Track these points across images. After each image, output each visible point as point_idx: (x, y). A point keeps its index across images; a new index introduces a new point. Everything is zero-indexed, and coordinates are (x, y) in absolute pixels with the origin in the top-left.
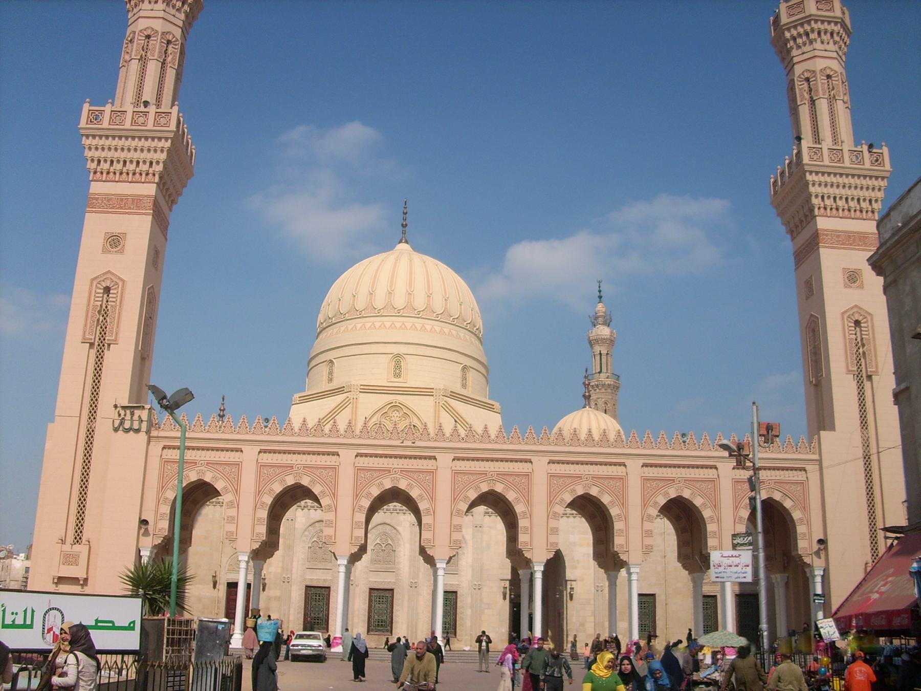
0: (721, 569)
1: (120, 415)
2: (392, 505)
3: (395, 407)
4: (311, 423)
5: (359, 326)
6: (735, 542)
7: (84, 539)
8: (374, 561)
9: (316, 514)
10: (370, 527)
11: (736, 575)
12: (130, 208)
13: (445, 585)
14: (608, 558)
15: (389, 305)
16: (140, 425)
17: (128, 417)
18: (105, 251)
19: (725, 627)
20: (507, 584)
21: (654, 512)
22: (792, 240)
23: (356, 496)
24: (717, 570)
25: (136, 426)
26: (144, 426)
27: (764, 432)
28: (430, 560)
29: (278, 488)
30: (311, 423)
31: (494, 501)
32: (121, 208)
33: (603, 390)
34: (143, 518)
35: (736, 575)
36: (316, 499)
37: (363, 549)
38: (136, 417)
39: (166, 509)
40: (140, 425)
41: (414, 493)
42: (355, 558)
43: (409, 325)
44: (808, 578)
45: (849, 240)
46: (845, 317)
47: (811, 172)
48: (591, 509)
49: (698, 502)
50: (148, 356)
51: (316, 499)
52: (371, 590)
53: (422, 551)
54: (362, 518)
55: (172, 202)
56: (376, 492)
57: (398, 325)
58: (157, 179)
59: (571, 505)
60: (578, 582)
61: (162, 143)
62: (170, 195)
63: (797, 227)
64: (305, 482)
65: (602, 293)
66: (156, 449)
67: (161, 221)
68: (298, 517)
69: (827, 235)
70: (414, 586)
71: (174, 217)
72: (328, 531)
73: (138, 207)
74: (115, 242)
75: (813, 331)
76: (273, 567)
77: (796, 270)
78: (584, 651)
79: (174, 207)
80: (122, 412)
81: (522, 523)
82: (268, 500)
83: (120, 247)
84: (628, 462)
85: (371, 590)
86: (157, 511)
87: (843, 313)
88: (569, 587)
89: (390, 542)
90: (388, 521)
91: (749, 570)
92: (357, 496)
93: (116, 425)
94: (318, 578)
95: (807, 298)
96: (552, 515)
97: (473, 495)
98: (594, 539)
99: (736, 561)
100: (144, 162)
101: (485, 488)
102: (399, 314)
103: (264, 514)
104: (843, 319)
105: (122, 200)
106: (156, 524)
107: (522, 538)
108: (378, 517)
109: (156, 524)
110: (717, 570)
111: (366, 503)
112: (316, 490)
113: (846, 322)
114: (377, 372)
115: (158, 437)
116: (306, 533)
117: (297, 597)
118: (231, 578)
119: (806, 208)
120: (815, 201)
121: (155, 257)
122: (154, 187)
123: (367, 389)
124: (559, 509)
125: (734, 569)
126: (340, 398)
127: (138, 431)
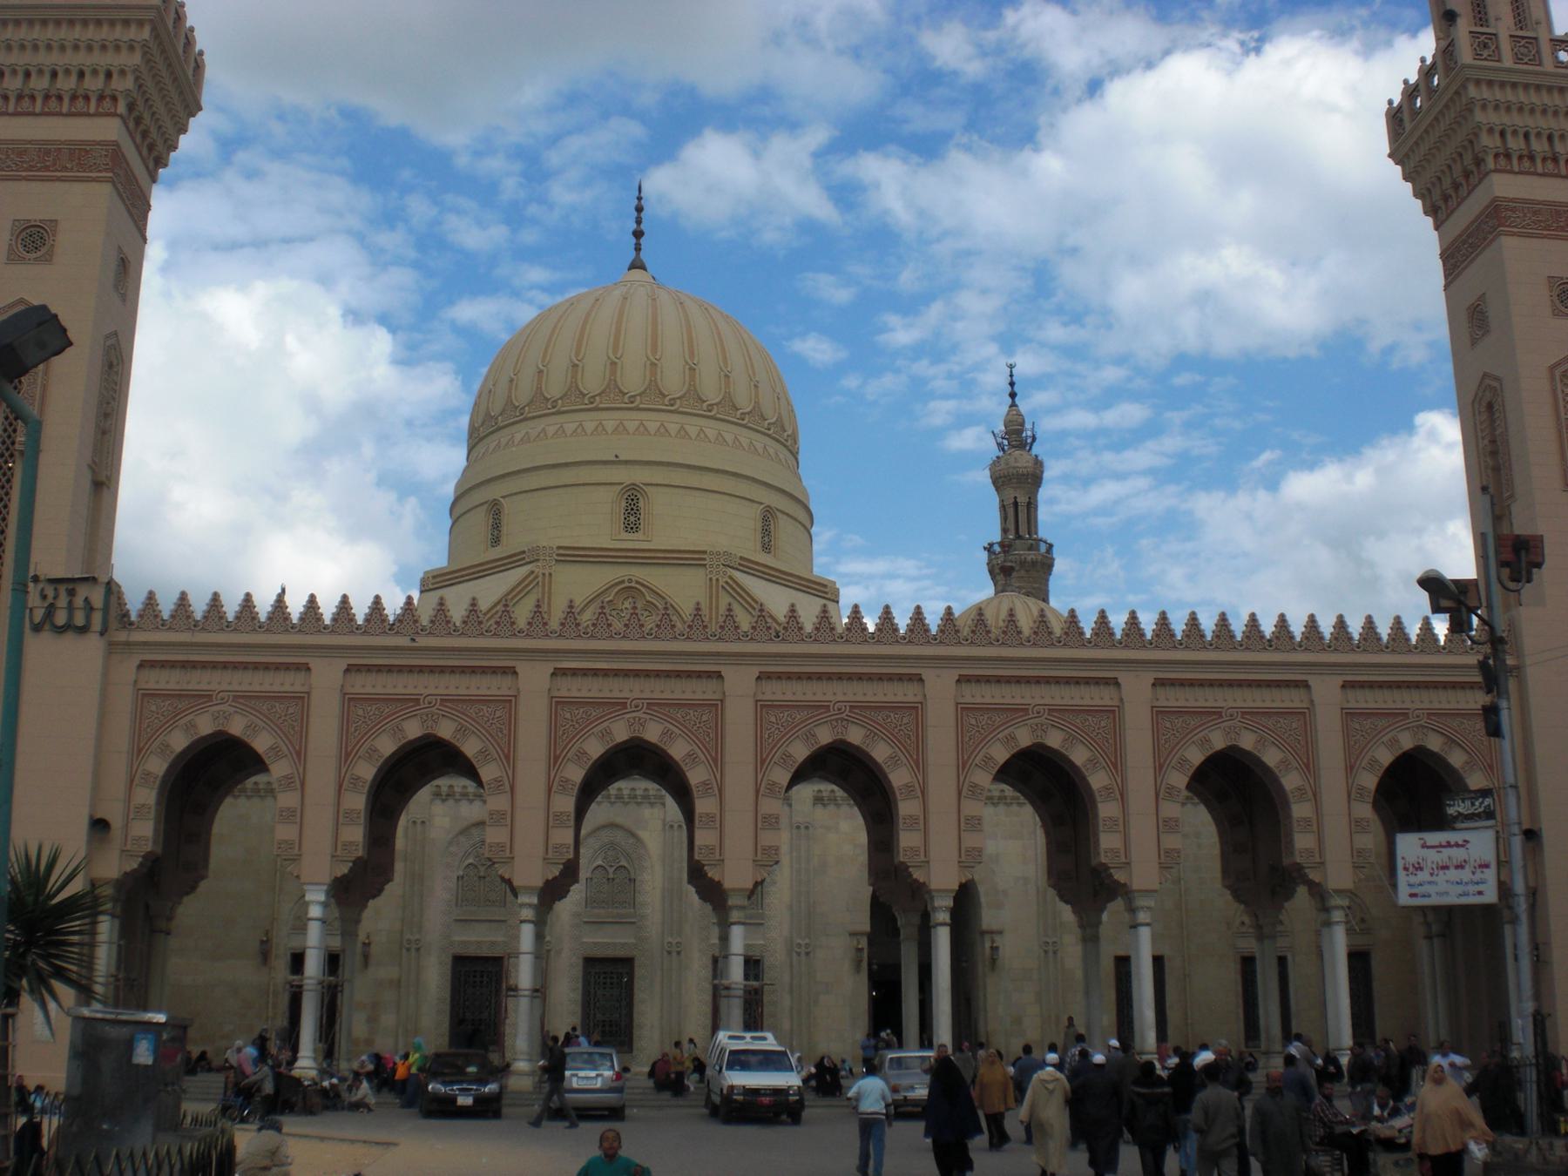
0: (1423, 876)
1: (44, 597)
2: (443, 783)
3: (630, 590)
5: (551, 430)
8: (590, 902)
9: (471, 811)
10: (583, 832)
11: (1460, 889)
12: (65, 169)
13: (747, 946)
14: (1081, 877)
15: (613, 387)
16: (88, 618)
17: (63, 601)
18: (13, 258)
20: (864, 943)
21: (1180, 780)
22: (1437, 228)
23: (555, 760)
24: (1412, 879)
25: (79, 620)
26: (97, 619)
27: (1508, 556)
28: (712, 892)
29: (387, 746)
31: (845, 768)
32: (47, 168)
33: (1023, 573)
34: (99, 816)
35: (1460, 889)
36: (470, 772)
37: (570, 872)
38: (79, 601)
39: (148, 796)
40: (88, 618)
41: (678, 751)
42: (553, 892)
43: (653, 427)
45: (521, 1074)
46: (1558, 373)
47: (1478, 82)
48: (1046, 781)
49: (1271, 758)
50: (108, 478)
51: (470, 772)
52: (590, 962)
53: (697, 874)
54: (567, 804)
56: (595, 749)
57: (631, 426)
58: (121, 108)
59: (1005, 773)
61: (132, 33)
62: (151, 148)
63: (1446, 198)
64: (445, 731)
65: (1016, 389)
66: (126, 669)
68: (434, 814)
69: (1513, 210)
70: (675, 951)
72: (495, 835)
75: (1490, 406)
76: (380, 916)
77: (1446, 287)
80: (50, 592)
81: (906, 808)
82: (367, 771)
83: (44, 250)
84: (1123, 677)
85: (590, 962)
86: (129, 799)
87: (1552, 368)
88: (988, 945)
89: (623, 863)
90: (619, 820)
91: (1490, 875)
92: (556, 758)
93: (37, 619)
94: (479, 939)
95: (1474, 342)
96: (964, 790)
97: (801, 752)
98: (1048, 844)
99: (1458, 854)
100: (95, 72)
101: (825, 737)
102: (631, 404)
103: (358, 801)
104: (1552, 378)
105: (48, 152)
106: (126, 826)
107: (907, 840)
108: (598, 812)
109: (126, 826)
110: (1412, 879)
111: (576, 774)
112: (470, 748)
113: (1559, 386)
114: (596, 524)
115: (128, 644)
116: (452, 849)
117: (435, 979)
118: (295, 943)
119: (1468, 159)
120: (1488, 141)
123: (573, 556)
124: (983, 778)
125: (1452, 874)
126: (521, 572)
127: (83, 630)
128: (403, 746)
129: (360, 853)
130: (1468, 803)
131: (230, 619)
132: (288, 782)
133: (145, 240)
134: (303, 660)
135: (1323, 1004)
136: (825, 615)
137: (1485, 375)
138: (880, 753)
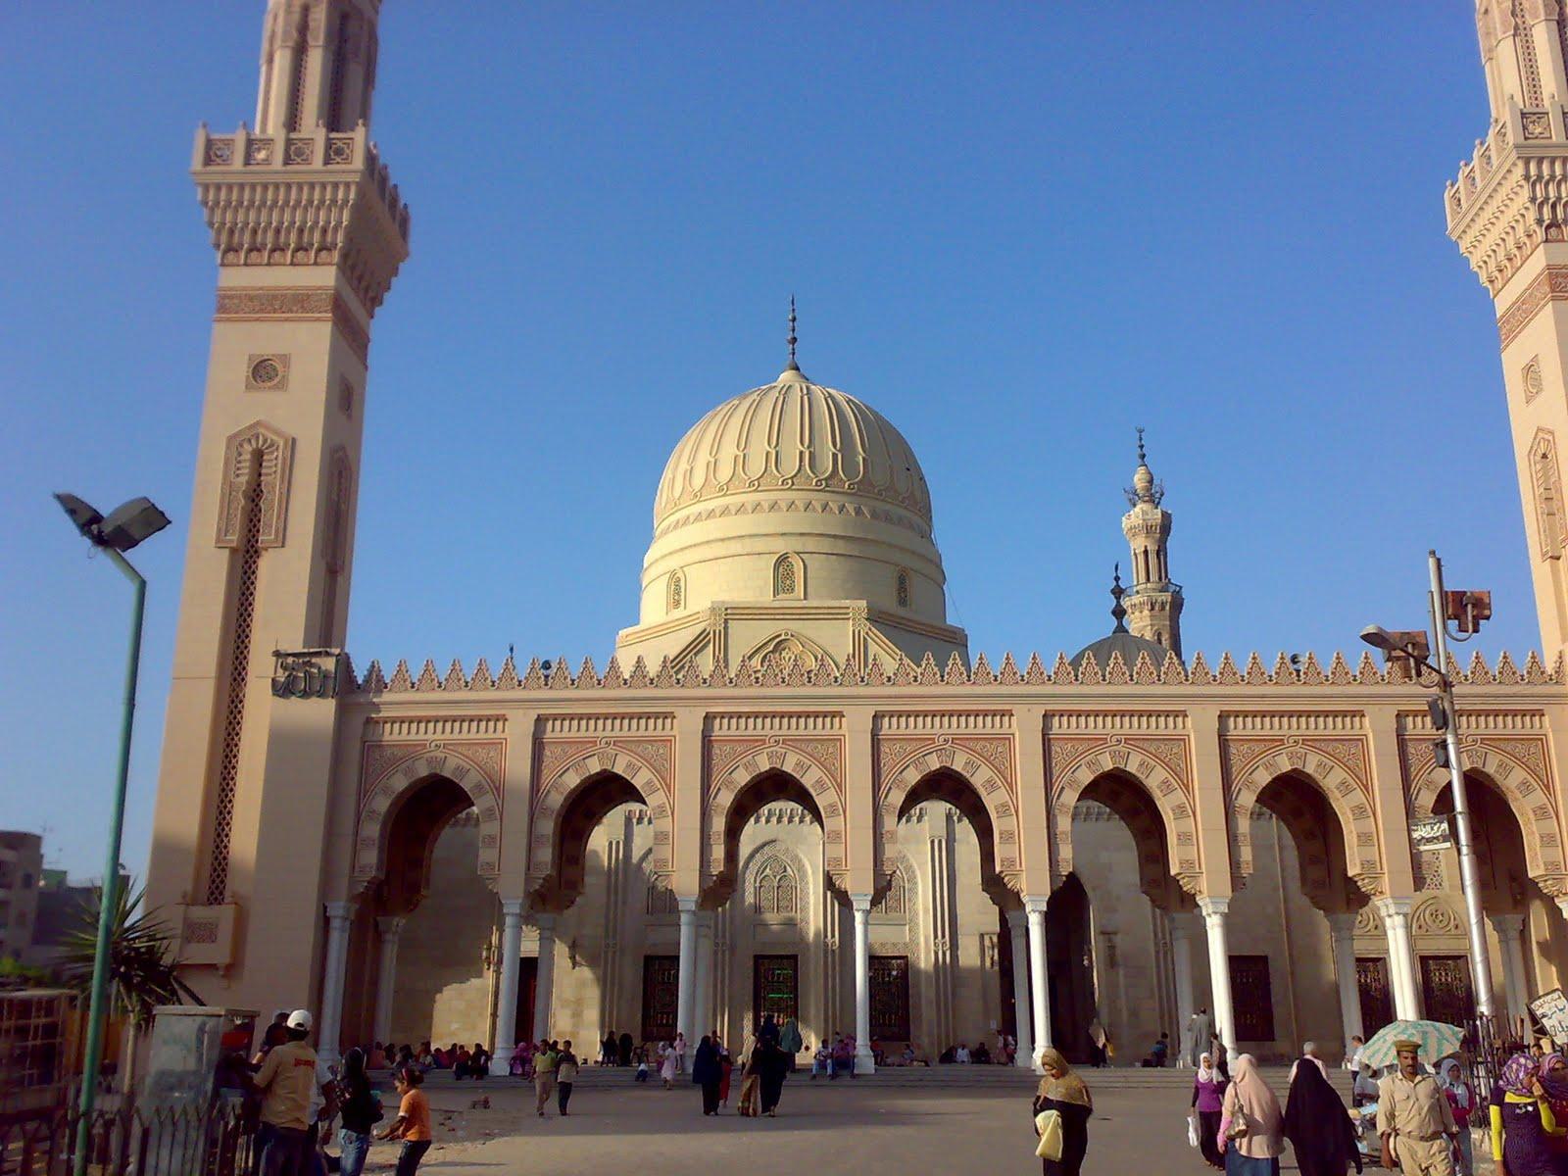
2: (776, 806)
4: (653, 668)
6: (1415, 835)
7: (227, 893)
19: (1400, 1015)
30: (653, 668)
31: (947, 786)
44: (958, 779)
55: (373, 299)
60: (1119, 936)
67: (351, 336)
71: (382, 327)
73: (304, 310)
74: (263, 372)
78: (378, 918)
79: (378, 310)
83: (276, 380)
121: (345, 398)
122: (332, 271)
128: (758, 775)
129: (722, 869)
130: (1428, 828)
131: (627, 677)
132: (489, 813)
133: (366, 368)
134: (502, 712)
135: (855, 1028)
136: (1535, 660)
137: (1539, 429)
138: (1153, 782)
